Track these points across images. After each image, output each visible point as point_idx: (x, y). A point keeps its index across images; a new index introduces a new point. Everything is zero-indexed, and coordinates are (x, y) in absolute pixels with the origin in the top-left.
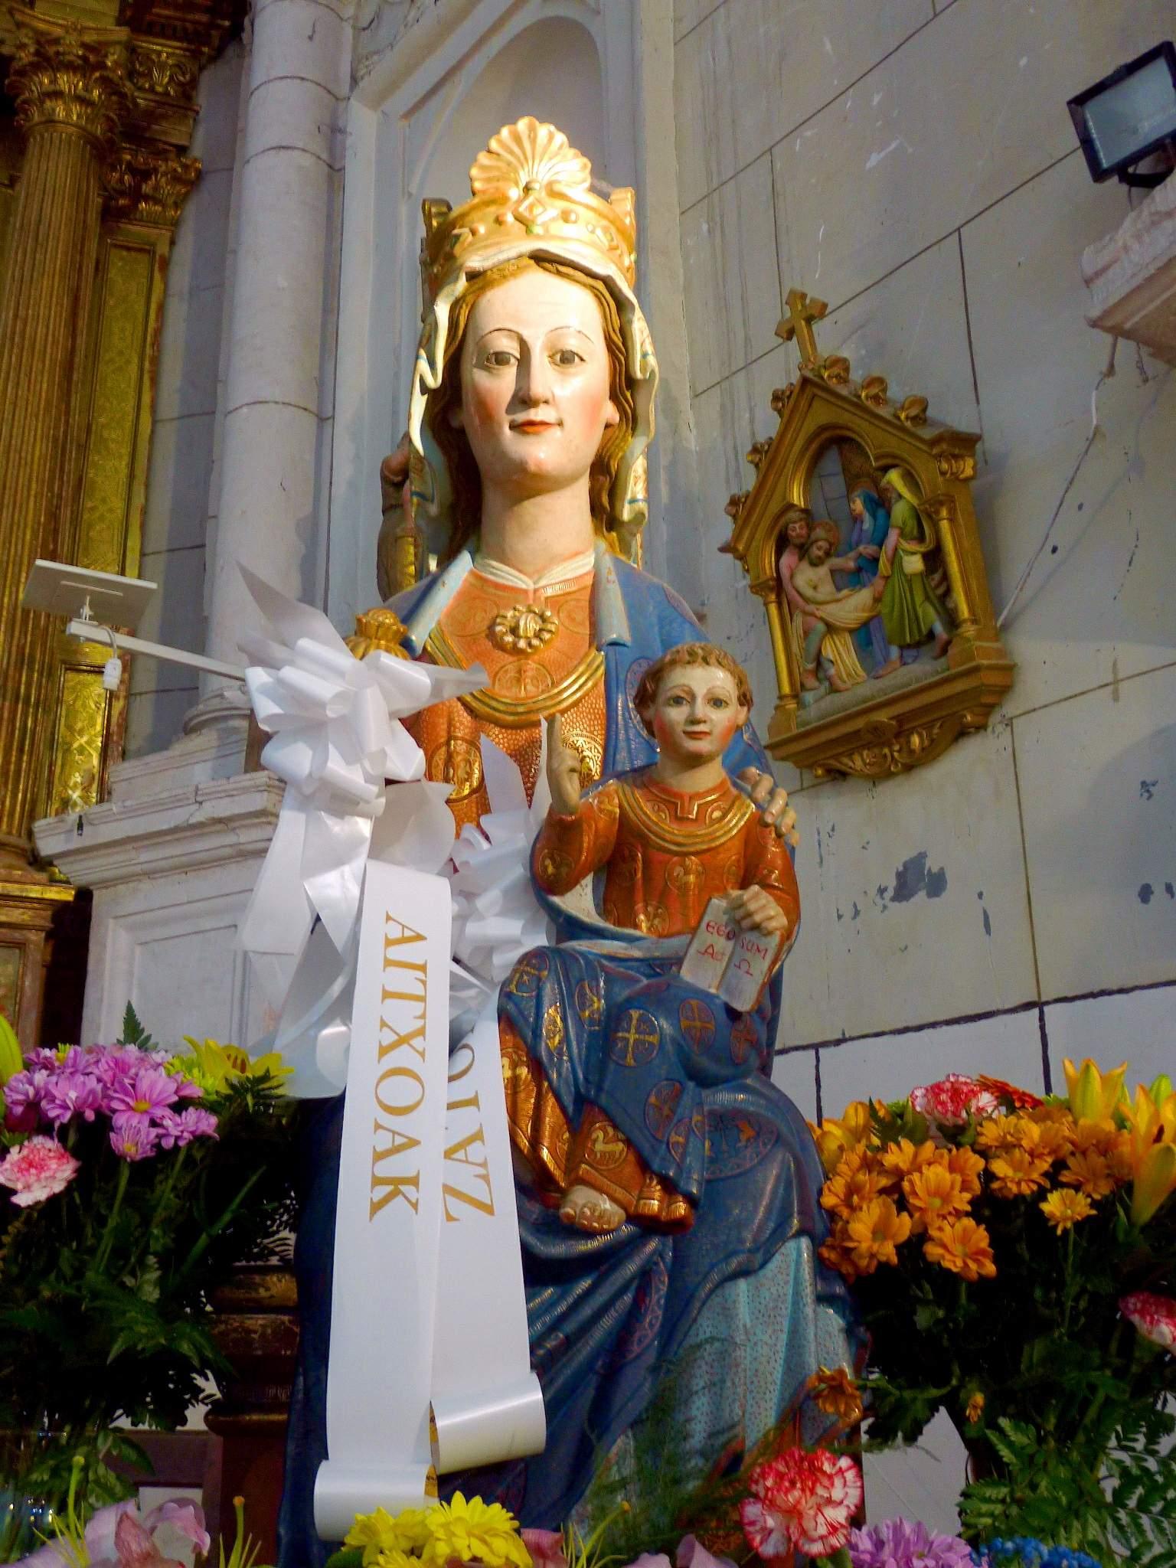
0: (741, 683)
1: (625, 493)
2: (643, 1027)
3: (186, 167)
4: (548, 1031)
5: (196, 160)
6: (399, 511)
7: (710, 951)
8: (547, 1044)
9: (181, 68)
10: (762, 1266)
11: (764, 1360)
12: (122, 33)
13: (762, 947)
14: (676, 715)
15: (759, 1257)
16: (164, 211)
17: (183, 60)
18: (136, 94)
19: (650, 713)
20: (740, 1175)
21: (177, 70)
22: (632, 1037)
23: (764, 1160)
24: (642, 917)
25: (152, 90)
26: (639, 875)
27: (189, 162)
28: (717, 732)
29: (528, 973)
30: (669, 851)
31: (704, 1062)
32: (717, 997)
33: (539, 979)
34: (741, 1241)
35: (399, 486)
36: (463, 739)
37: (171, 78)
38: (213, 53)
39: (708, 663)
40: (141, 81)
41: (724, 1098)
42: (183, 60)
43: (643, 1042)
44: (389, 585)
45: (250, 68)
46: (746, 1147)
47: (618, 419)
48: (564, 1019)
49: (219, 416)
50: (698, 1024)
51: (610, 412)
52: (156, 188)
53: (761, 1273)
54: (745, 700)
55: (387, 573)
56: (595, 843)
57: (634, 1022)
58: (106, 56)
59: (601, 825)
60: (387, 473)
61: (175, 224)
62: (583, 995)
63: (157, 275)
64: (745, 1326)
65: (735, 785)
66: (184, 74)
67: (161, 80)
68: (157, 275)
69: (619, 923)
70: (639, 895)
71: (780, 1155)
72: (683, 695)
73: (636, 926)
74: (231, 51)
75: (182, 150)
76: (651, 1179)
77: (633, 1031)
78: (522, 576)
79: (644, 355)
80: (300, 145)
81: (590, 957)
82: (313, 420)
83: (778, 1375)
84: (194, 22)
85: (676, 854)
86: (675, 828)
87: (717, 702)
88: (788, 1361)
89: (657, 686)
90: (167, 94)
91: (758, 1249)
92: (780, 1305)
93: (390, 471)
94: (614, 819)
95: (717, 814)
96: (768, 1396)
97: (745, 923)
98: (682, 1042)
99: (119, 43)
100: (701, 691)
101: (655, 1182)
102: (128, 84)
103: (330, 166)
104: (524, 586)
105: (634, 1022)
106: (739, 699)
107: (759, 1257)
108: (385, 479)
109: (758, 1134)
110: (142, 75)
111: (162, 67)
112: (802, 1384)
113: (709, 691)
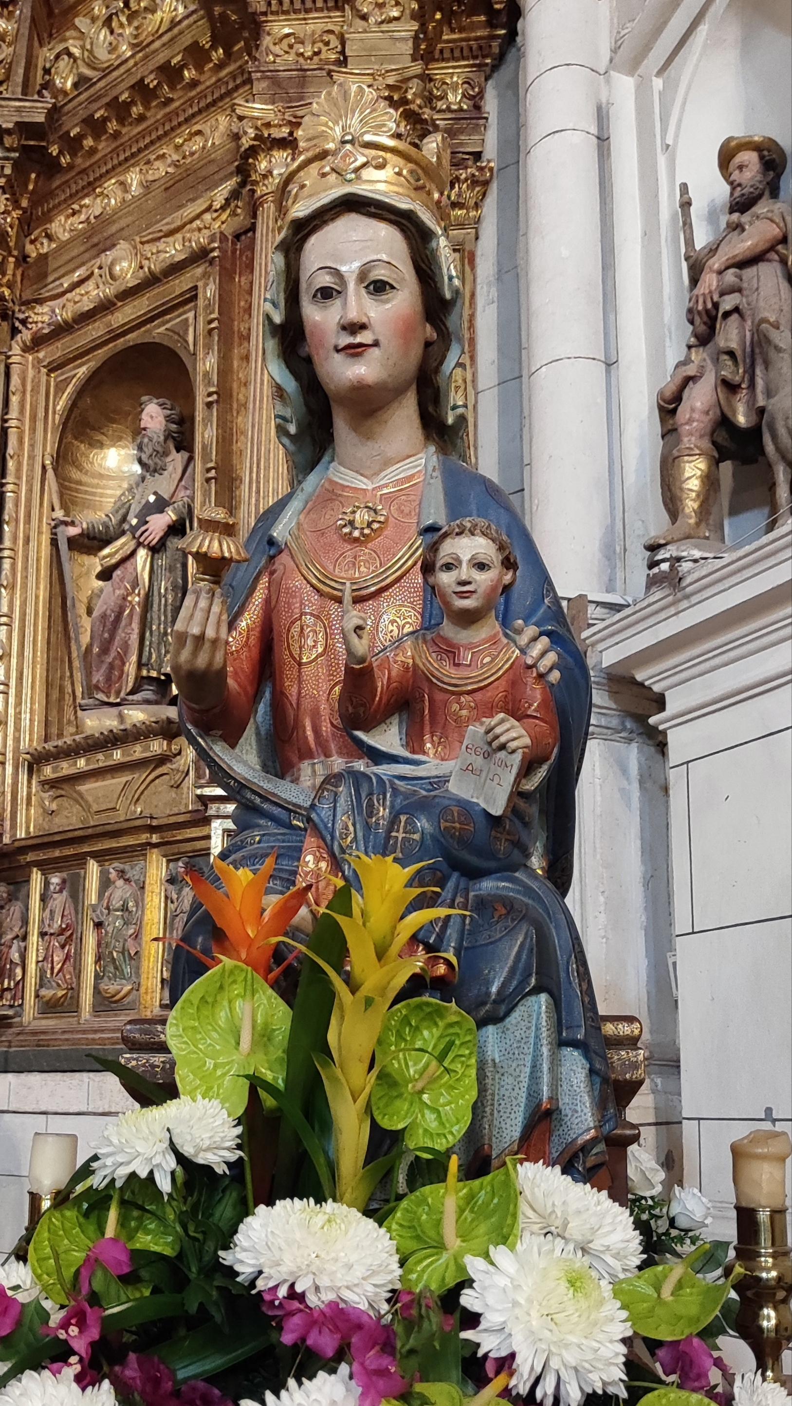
0: (501, 548)
1: (448, 401)
2: (409, 828)
3: (481, 169)
4: (341, 834)
5: (489, 161)
6: (674, 434)
7: (470, 768)
8: (340, 844)
9: (468, 83)
10: (508, 1014)
11: (509, 1087)
12: (417, 68)
13: (508, 764)
14: (446, 579)
15: (503, 1009)
16: (468, 212)
17: (470, 75)
18: (435, 117)
19: (431, 580)
20: (491, 943)
21: (466, 86)
22: (401, 835)
23: (511, 932)
24: (429, 745)
25: (449, 109)
26: (427, 712)
27: (484, 164)
28: (480, 591)
29: (328, 790)
30: (447, 691)
31: (466, 856)
32: (478, 805)
33: (336, 794)
34: (488, 994)
35: (674, 412)
36: (311, 614)
37: (464, 96)
38: (496, 62)
39: (473, 534)
40: (439, 104)
41: (487, 885)
42: (470, 75)
43: (409, 840)
44: (671, 499)
45: (525, 68)
46: (498, 922)
47: (435, 335)
48: (354, 825)
49: (525, 379)
50: (457, 825)
51: (430, 332)
52: (459, 195)
53: (508, 1020)
54: (509, 564)
55: (670, 490)
56: (388, 687)
57: (402, 824)
58: (406, 91)
59: (394, 673)
60: (662, 403)
61: (478, 221)
62: (371, 805)
63: (467, 268)
64: (493, 1060)
65: (506, 635)
66: (473, 88)
67: (454, 98)
68: (467, 268)
69: (413, 752)
70: (427, 728)
71: (524, 927)
72: (450, 561)
73: (424, 753)
74: (511, 55)
75: (478, 156)
76: (418, 947)
77: (401, 830)
78: (362, 478)
79: (451, 278)
80: (571, 126)
81: (384, 777)
82: (603, 366)
83: (523, 1100)
84: (476, 39)
85: (453, 693)
86: (453, 671)
87: (482, 566)
88: (529, 1088)
89: (435, 556)
90: (461, 110)
91: (503, 1001)
92: (522, 1045)
93: (664, 401)
94: (408, 668)
95: (487, 659)
96: (513, 1116)
97: (495, 744)
98: (442, 840)
99: (415, 77)
100: (465, 558)
101: (421, 948)
102: (427, 110)
103: (598, 138)
104: (364, 487)
105: (402, 824)
106: (502, 563)
107: (503, 1009)
108: (661, 409)
109: (508, 913)
110: (440, 98)
111: (455, 89)
112: (539, 1105)
113: (473, 558)
